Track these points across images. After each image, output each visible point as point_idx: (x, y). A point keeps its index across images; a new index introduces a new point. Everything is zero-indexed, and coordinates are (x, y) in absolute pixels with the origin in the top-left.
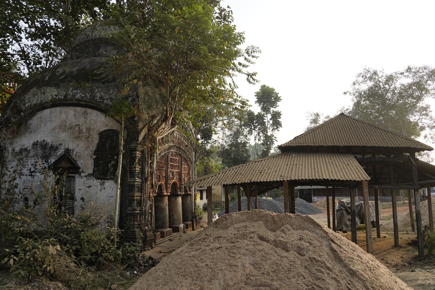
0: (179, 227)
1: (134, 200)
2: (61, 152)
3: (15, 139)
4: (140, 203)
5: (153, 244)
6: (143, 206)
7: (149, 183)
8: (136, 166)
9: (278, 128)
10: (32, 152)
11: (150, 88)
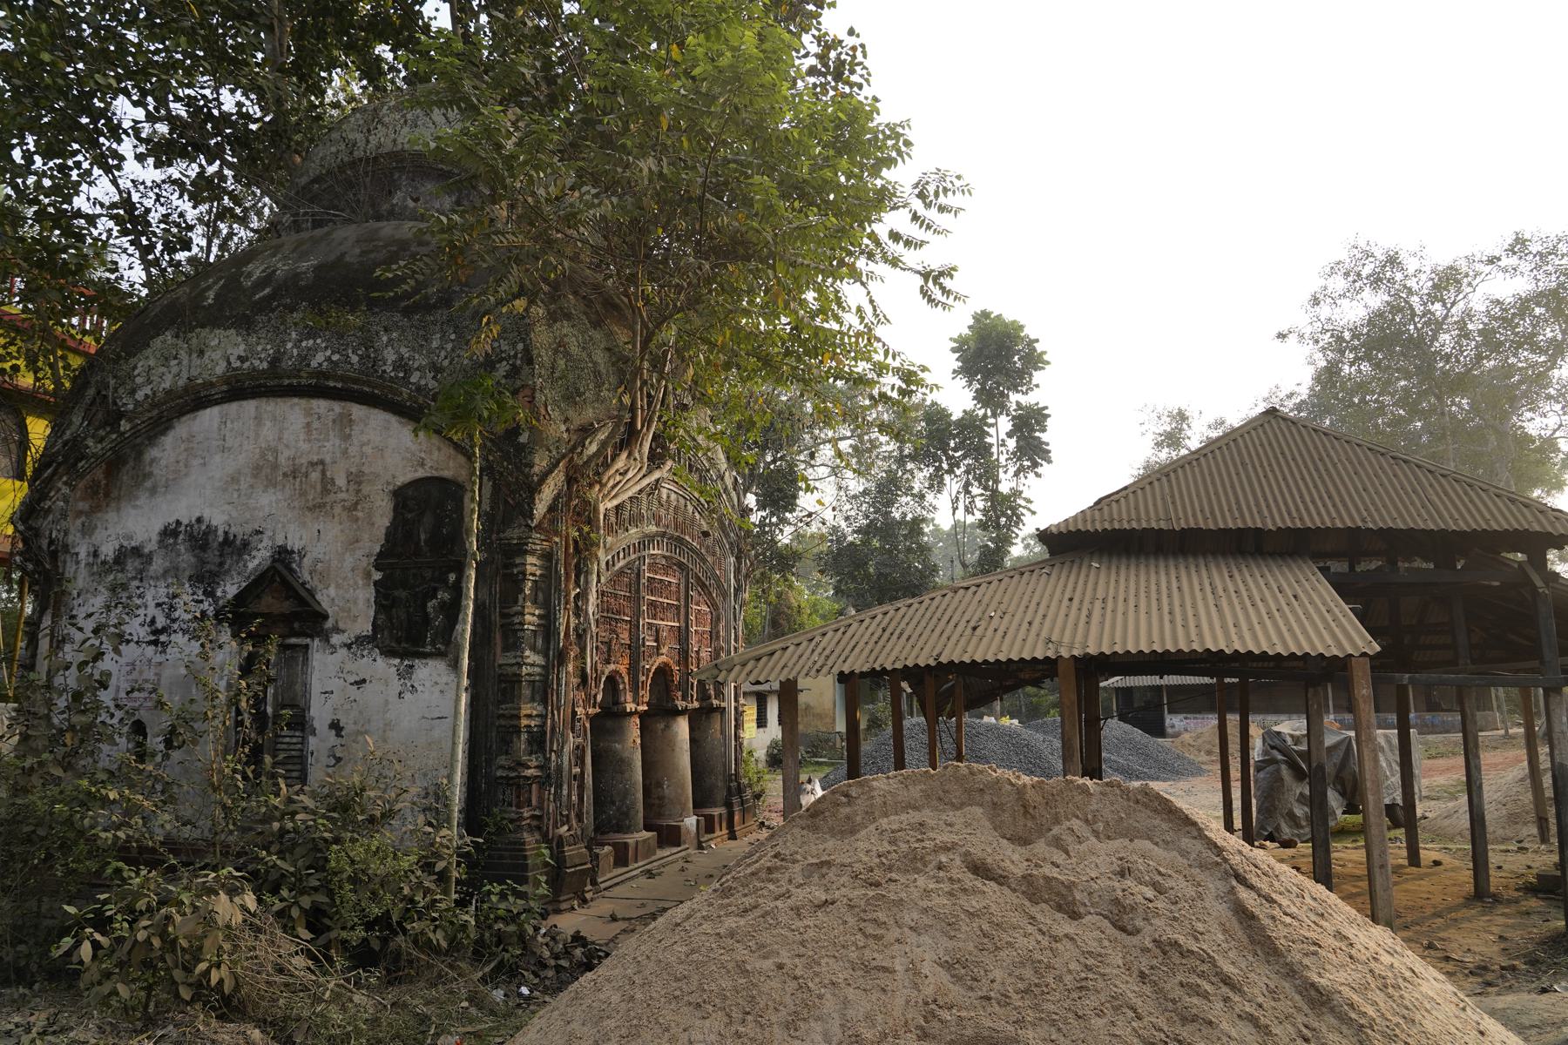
0: (679, 827)
2: (259, 559)
3: (99, 515)
4: (538, 741)
5: (589, 887)
6: (551, 750)
7: (570, 668)
9: (1035, 465)
10: (160, 561)
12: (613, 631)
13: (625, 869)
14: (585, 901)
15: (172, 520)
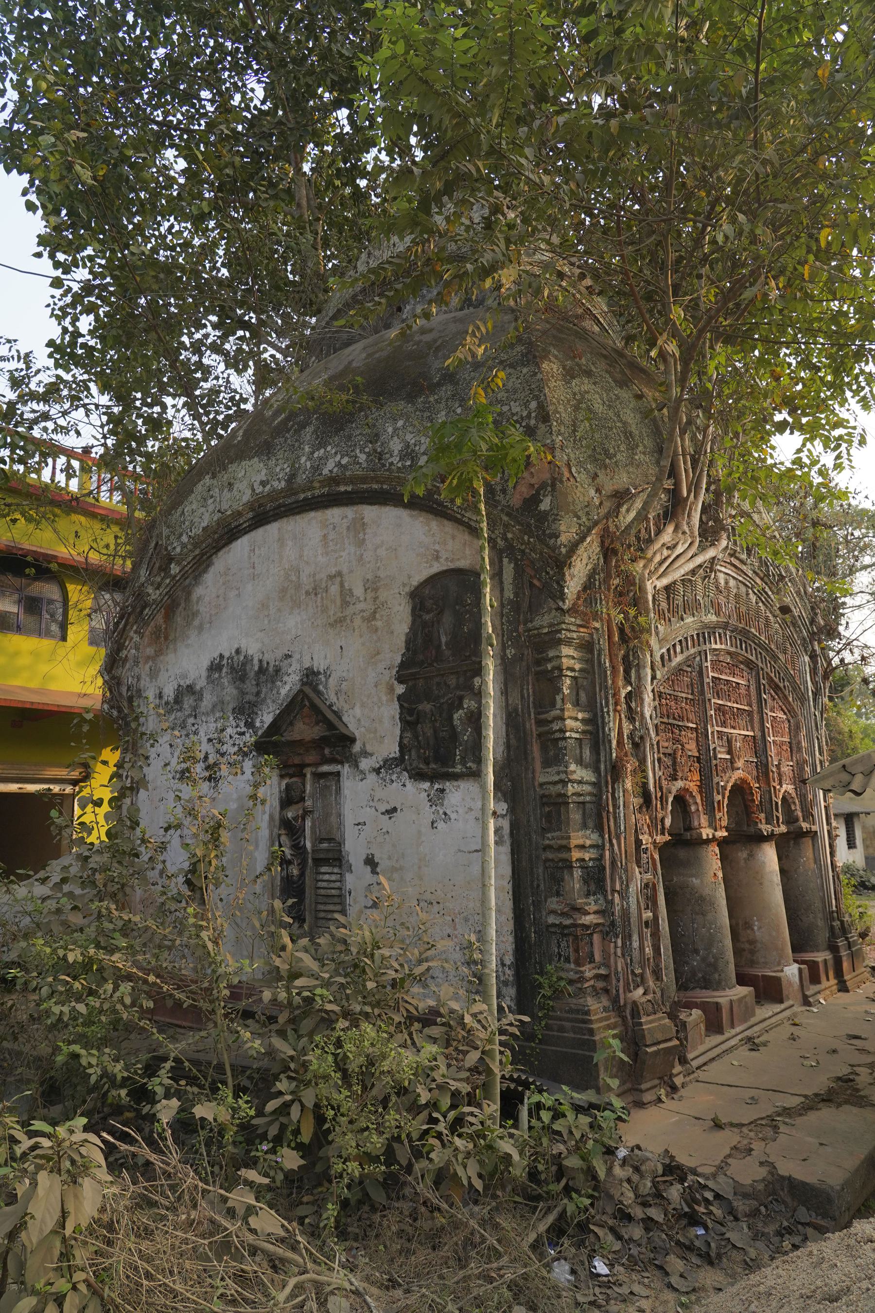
0: (778, 980)
3: (161, 658)
5: (678, 1069)
6: (614, 891)
7: (628, 785)
8: (562, 710)
10: (209, 697)
11: (595, 383)
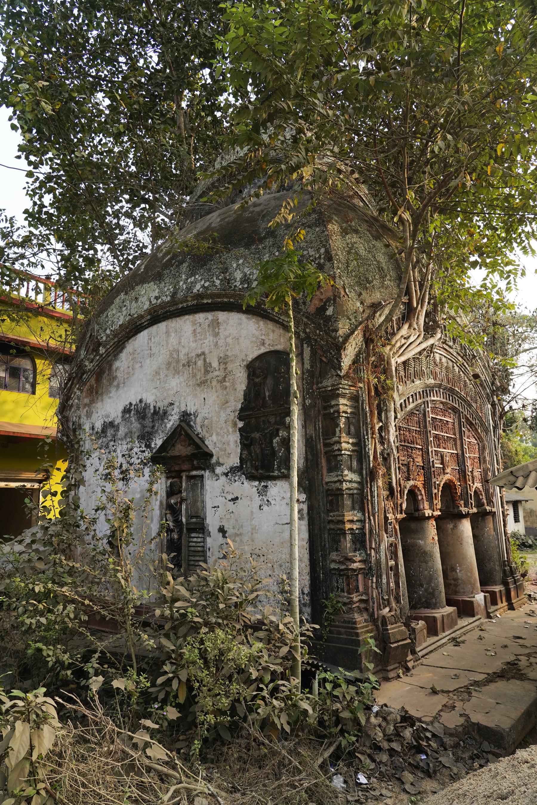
0: (472, 603)
1: (345, 534)
5: (410, 657)
6: (371, 548)
7: (380, 483)
8: (340, 437)
11: (360, 238)
12: (410, 456)
13: (436, 638)
14: (408, 669)
15: (127, 403)
